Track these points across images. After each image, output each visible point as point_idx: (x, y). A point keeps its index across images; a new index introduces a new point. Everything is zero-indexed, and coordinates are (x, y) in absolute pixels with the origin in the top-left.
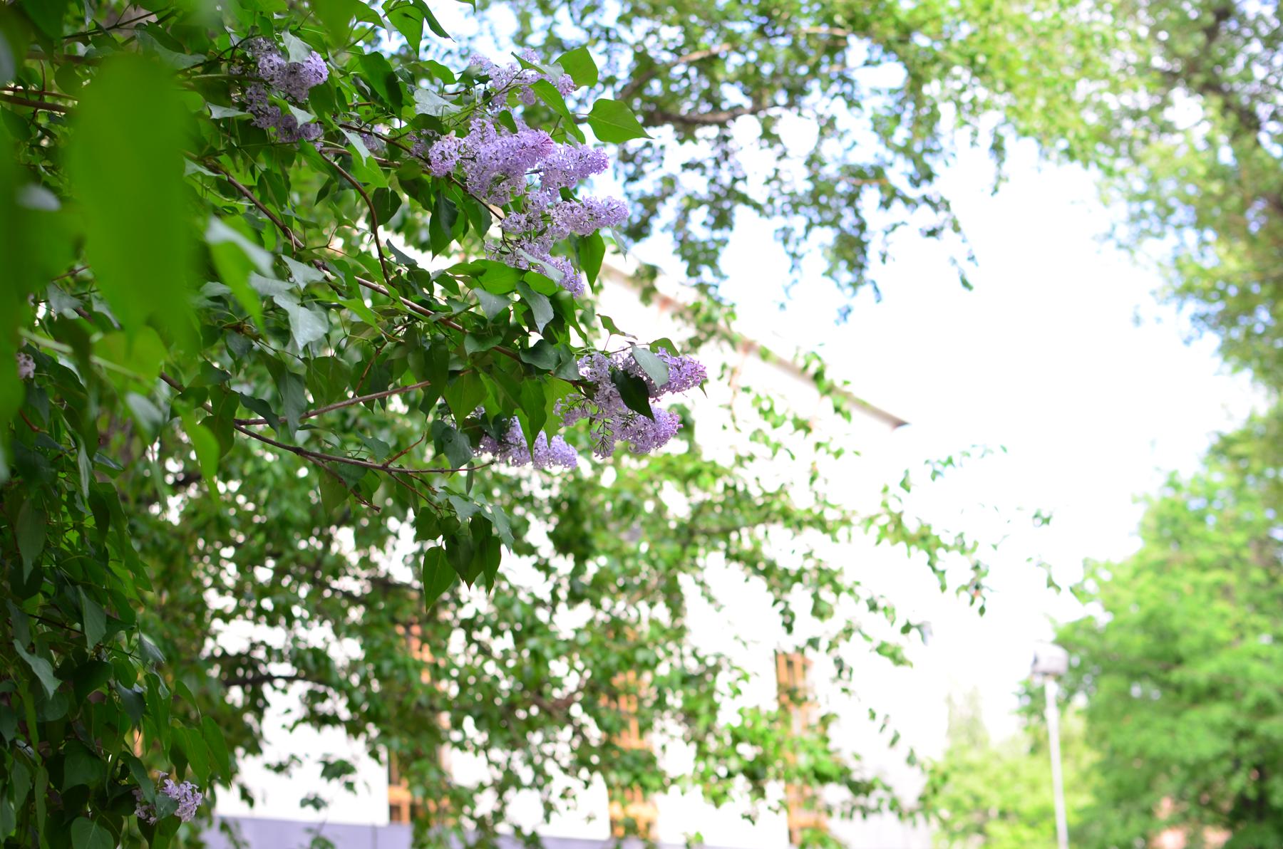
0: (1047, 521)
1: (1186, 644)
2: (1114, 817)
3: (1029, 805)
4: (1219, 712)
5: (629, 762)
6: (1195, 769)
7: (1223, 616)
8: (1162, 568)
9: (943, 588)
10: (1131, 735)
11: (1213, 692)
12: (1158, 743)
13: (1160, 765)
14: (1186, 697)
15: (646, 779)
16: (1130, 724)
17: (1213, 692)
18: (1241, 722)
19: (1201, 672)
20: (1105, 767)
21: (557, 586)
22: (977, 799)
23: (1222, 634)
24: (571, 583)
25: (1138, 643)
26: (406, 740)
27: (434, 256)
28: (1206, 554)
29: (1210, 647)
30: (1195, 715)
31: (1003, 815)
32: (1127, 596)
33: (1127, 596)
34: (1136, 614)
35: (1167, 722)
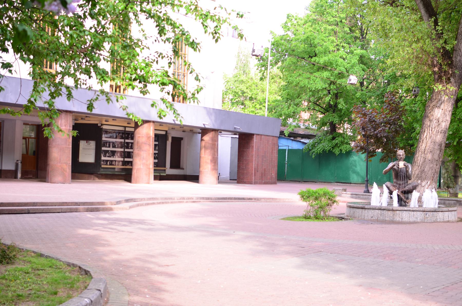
0: (242, 16)
1: (319, 49)
2: (285, 105)
3: (260, 97)
4: (326, 74)
5: (101, 72)
6: (314, 92)
7: (333, 42)
8: (315, 21)
9: (205, 32)
10: (295, 78)
11: (324, 68)
12: (304, 82)
13: (304, 89)
14: (315, 68)
15: (105, 78)
16: (296, 74)
17: (324, 68)
18: (332, 79)
19: (322, 60)
20: (285, 88)
21: (85, 12)
22: (243, 93)
23: (331, 48)
24: (90, 11)
25: (302, 47)
26: (55, 18)
27: (2, 52)
28: (331, 19)
29: (326, 52)
30: (317, 74)
31: (251, 99)
32: (301, 30)
33: (301, 30)
34: (303, 37)
35: (308, 75)
